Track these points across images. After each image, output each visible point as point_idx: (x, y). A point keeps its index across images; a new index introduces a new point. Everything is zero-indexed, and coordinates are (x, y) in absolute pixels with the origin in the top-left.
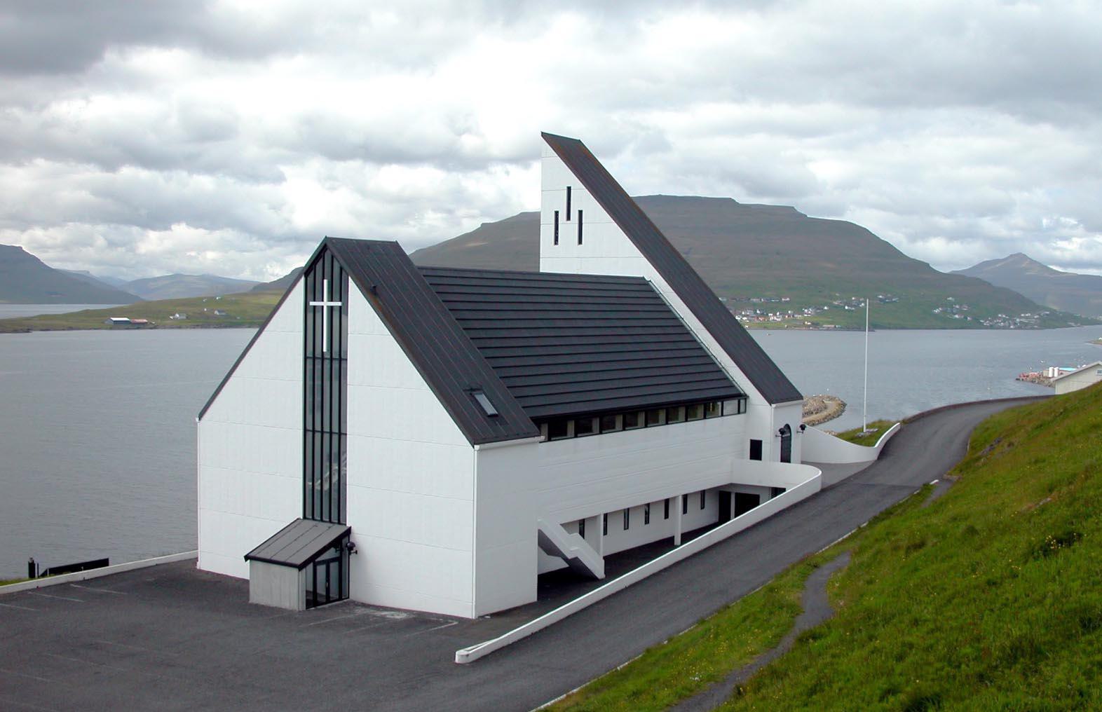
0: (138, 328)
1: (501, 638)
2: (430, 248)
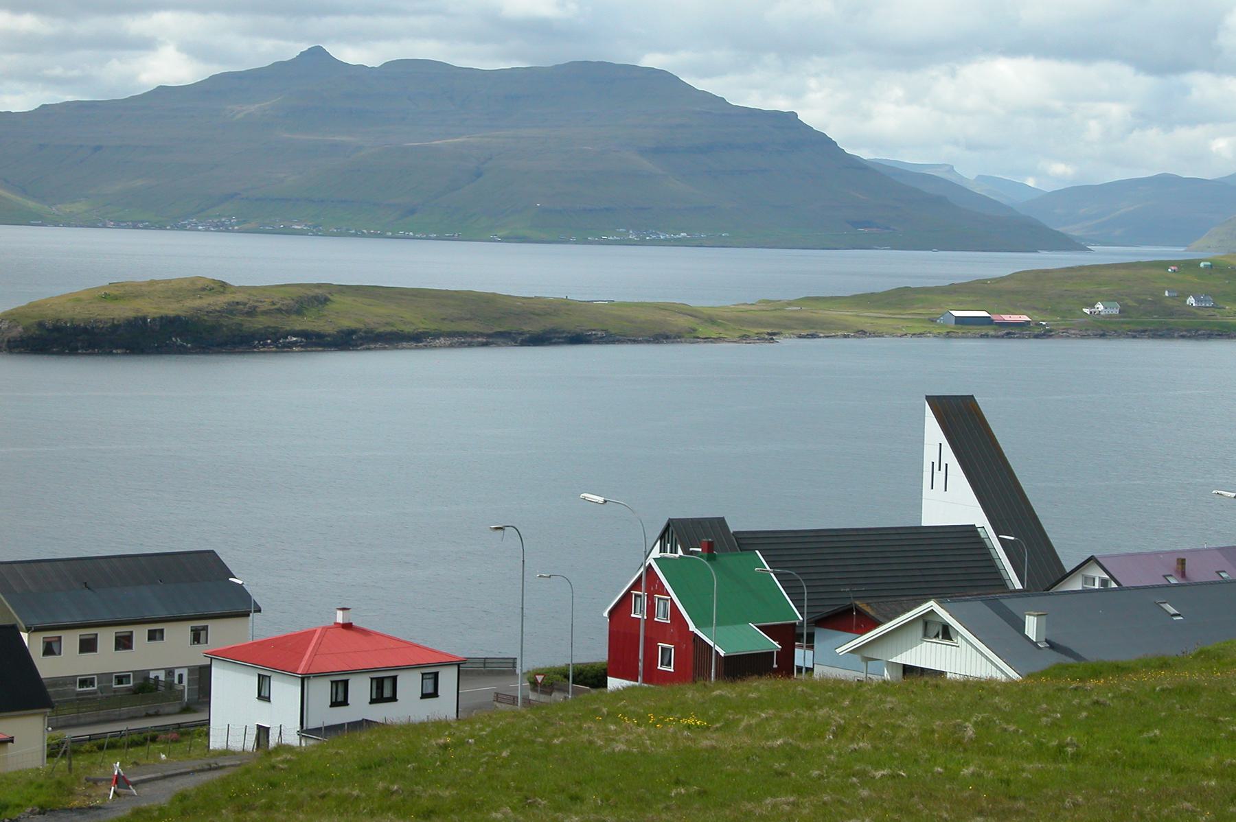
0: (1009, 335)
1: (641, 656)
2: (557, 67)
